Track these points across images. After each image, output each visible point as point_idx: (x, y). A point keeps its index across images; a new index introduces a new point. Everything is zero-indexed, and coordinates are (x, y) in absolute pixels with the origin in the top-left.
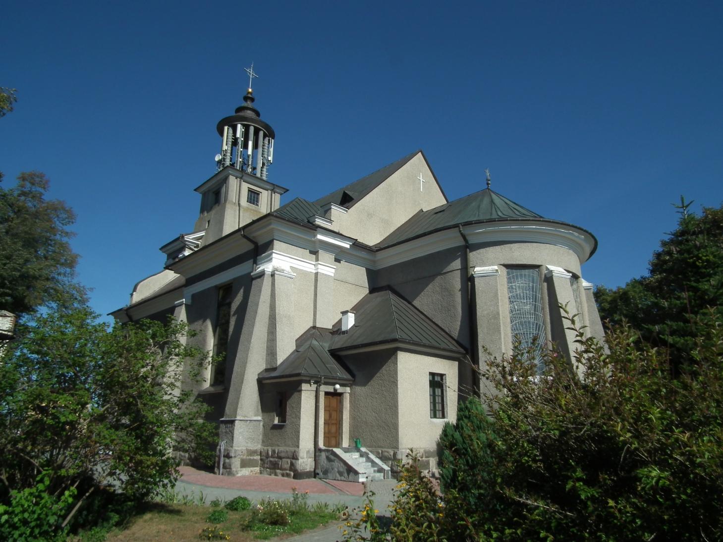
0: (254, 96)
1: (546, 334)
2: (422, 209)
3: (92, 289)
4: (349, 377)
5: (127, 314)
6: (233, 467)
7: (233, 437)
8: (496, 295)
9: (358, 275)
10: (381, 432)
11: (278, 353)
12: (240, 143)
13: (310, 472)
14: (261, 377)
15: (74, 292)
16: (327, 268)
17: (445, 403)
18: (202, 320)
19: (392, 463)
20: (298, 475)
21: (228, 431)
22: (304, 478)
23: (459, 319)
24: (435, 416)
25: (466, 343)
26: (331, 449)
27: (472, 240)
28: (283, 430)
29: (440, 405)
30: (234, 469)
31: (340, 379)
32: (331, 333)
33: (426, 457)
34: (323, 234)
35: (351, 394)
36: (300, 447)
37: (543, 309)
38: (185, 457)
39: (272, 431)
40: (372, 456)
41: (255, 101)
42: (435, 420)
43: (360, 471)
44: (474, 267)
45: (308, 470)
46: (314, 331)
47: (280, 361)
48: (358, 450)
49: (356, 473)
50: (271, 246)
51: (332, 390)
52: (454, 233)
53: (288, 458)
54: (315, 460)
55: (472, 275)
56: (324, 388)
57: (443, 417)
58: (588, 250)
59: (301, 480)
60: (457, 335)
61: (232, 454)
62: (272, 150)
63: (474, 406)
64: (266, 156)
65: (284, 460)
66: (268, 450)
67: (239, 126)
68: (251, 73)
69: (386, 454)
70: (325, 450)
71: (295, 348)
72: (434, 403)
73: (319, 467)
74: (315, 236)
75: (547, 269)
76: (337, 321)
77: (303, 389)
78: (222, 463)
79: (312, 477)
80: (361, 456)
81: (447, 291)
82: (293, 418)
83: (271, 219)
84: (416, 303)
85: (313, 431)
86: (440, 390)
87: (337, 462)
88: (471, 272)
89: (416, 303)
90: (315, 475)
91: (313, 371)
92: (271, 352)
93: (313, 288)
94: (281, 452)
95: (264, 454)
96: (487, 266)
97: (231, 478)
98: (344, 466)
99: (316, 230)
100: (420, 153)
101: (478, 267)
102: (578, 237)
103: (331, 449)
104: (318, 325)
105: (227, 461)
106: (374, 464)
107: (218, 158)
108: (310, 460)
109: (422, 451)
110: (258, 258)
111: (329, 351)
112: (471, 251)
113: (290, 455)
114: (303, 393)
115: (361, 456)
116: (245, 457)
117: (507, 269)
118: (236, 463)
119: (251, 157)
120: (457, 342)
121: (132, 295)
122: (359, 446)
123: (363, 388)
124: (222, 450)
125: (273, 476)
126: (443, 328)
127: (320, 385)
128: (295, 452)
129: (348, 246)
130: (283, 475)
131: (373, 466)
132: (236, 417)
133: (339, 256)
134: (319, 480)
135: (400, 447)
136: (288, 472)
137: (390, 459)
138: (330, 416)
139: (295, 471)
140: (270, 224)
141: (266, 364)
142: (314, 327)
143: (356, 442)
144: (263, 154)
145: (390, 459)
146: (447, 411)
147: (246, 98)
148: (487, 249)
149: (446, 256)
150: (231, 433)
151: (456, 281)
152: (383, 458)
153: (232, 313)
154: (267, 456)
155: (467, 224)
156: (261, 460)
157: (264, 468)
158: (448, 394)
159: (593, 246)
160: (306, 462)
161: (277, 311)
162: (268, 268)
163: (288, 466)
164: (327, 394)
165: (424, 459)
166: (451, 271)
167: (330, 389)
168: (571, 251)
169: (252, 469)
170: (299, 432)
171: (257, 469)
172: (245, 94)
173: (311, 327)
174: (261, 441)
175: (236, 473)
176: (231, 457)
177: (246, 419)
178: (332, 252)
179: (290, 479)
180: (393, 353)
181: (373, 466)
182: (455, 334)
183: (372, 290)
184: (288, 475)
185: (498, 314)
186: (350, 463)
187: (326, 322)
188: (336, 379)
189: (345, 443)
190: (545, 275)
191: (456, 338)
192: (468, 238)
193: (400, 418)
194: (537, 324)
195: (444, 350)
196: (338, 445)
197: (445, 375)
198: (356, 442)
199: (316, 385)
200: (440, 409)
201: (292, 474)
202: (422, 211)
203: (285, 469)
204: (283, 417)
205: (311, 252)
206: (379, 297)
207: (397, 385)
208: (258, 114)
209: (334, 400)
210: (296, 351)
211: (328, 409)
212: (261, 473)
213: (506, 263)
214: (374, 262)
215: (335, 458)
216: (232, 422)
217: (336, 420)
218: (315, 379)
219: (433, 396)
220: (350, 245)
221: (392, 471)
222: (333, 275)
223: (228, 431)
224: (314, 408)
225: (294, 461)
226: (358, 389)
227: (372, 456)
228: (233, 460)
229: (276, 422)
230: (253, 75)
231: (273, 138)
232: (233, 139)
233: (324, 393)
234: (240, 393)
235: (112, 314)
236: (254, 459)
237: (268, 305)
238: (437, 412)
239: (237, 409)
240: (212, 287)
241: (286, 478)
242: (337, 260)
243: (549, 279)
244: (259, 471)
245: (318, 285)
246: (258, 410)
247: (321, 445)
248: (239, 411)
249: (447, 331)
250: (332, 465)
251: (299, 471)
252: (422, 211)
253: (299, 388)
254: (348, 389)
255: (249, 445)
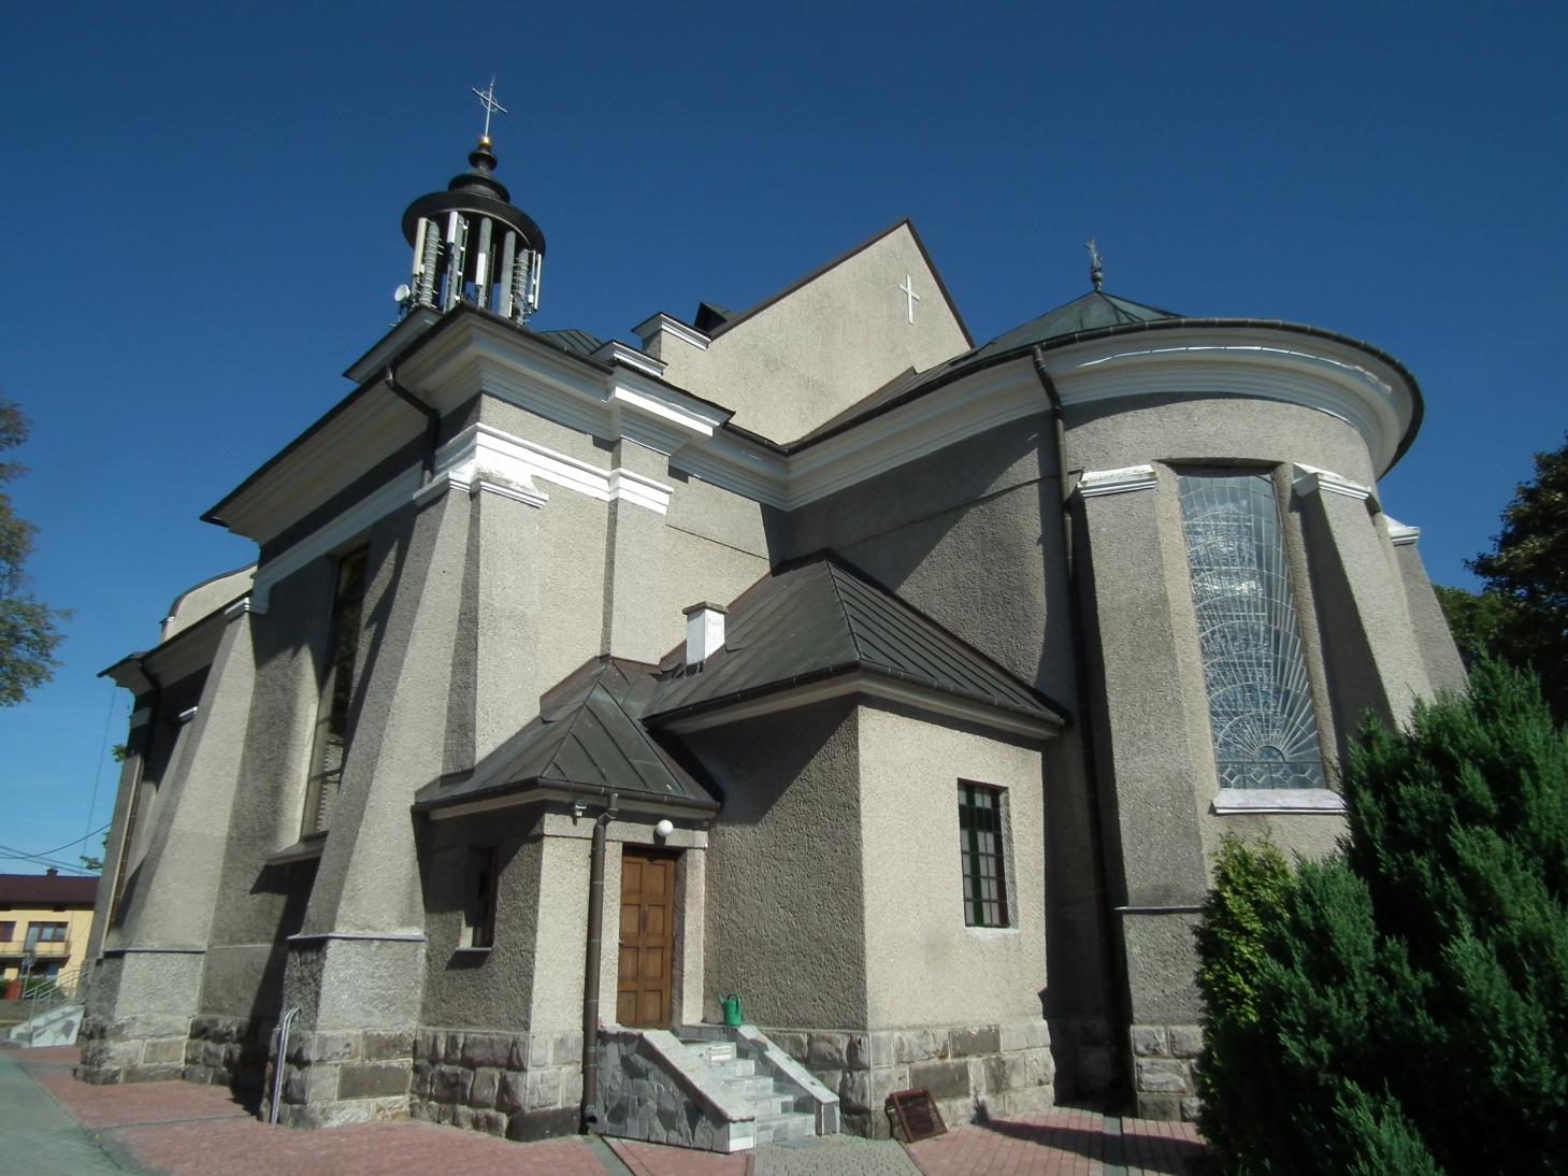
0: (495, 153)
1: (1306, 662)
2: (912, 369)
3: (67, 614)
4: (704, 797)
5: (144, 671)
6: (310, 1095)
7: (318, 994)
8: (1154, 544)
9: (739, 520)
10: (807, 981)
11: (479, 725)
12: (457, 257)
13: (566, 1112)
14: (423, 799)
15: (20, 620)
16: (645, 489)
17: (1007, 880)
18: (289, 652)
19: (844, 1080)
20: (523, 1127)
21: (306, 974)
22: (543, 1137)
23: (1040, 622)
24: (978, 920)
25: (1065, 695)
26: (636, 1031)
27: (1071, 395)
28: (482, 970)
29: (993, 884)
30: (314, 1105)
31: (672, 804)
32: (654, 675)
33: (958, 1055)
34: (632, 387)
35: (709, 852)
36: (535, 1025)
37: (1292, 589)
38: (217, 1056)
39: (452, 973)
40: (777, 1055)
41: (499, 165)
42: (978, 931)
43: (732, 1114)
44: (1081, 472)
45: (560, 1106)
46: (606, 668)
47: (483, 750)
48: (732, 1034)
49: (720, 1119)
50: (474, 414)
51: (649, 840)
52: (1019, 375)
53: (495, 1064)
54: (584, 1071)
55: (1077, 490)
56: (620, 832)
57: (1004, 922)
58: (1394, 436)
59: (531, 1145)
60: (1034, 673)
61: (312, 1054)
62: (536, 282)
63: (197, 1129)
64: (522, 293)
65: (480, 1070)
66: (435, 1038)
67: (454, 216)
68: (489, 100)
69: (824, 1047)
70: (617, 1037)
71: (537, 712)
72: (974, 878)
73: (599, 1094)
74: (608, 392)
75: (1299, 472)
76: (676, 645)
77: (547, 831)
78: (280, 1082)
79: (573, 1133)
80: (742, 1054)
81: (1004, 549)
82: (513, 928)
83: (470, 325)
84: (906, 590)
85: (582, 973)
86: (990, 837)
87: (658, 1079)
88: (1071, 484)
89: (906, 590)
90: (583, 1122)
91: (583, 775)
92: (461, 725)
93: (603, 544)
94: (475, 1043)
95: (424, 1050)
96: (1115, 465)
97: (304, 1137)
98: (677, 1092)
99: (611, 373)
100: (905, 225)
101: (1092, 470)
102: (1376, 387)
103: (636, 1031)
104: (616, 652)
105: (296, 1075)
106: (782, 1080)
107: (402, 293)
108: (566, 1069)
109: (942, 1034)
110: (438, 452)
111: (645, 721)
112: (1068, 427)
113: (501, 1053)
114: (549, 849)
115: (742, 1054)
116: (357, 1062)
117: (1179, 473)
118: (323, 1083)
119: (482, 292)
120: (1038, 695)
121: (164, 623)
122: (736, 1020)
123: (749, 829)
124: (285, 1038)
125: (446, 1128)
126: (991, 655)
127: (606, 822)
128: (514, 1044)
129: (709, 431)
130: (476, 1124)
131: (779, 1090)
132: (332, 929)
133: (685, 458)
134: (598, 1141)
135: (871, 1023)
136: (492, 1112)
137: (834, 1064)
138: (643, 922)
139: (513, 1109)
140: (468, 342)
141: (445, 762)
142: (605, 658)
143: (725, 1007)
144: (513, 287)
145: (834, 1064)
146: (1015, 905)
147: (475, 159)
148: (1119, 417)
149: (998, 446)
150: (314, 979)
151: (1027, 517)
152: (812, 1061)
153: (364, 622)
154: (434, 1060)
155: (1053, 344)
156: (416, 1069)
157: (422, 1096)
158: (1016, 852)
159: (1409, 416)
160: (551, 1079)
161: (482, 598)
162: (462, 474)
163: (490, 1093)
164: (630, 850)
165: (949, 1060)
166: (1011, 489)
167: (642, 834)
168: (1355, 432)
169: (380, 1100)
170: (530, 976)
171: (402, 1101)
172: (473, 148)
173: (596, 657)
174: (419, 1007)
175: (319, 1117)
176: (308, 1063)
177: (370, 934)
178: (659, 445)
179: (497, 1139)
180: (842, 712)
181: (779, 1090)
182: (1030, 671)
183: (779, 566)
184: (491, 1125)
185: (1164, 599)
186: (699, 1081)
187: (643, 644)
188: (659, 802)
189: (692, 1011)
190: (1294, 491)
191: (1032, 682)
192: (1060, 388)
193: (869, 924)
194: (1277, 633)
195: (1003, 710)
196: (666, 1019)
197: (1006, 788)
198: (725, 1007)
199: (592, 822)
200: (994, 896)
201: (504, 1120)
202: (912, 369)
203: (484, 1105)
204: (483, 921)
205: (599, 443)
206: (798, 578)
207: (857, 816)
208: (503, 194)
209: (655, 873)
210: (543, 720)
211: (634, 899)
212: (412, 1114)
213: (1175, 456)
214: (785, 487)
215: (650, 1065)
216: (319, 945)
217: (663, 934)
218: (592, 801)
219: (972, 854)
220: (715, 429)
221: (846, 1106)
222: (663, 510)
223: (306, 974)
224: (585, 896)
225: (510, 1075)
226: (736, 835)
227: (777, 1055)
228: (313, 1073)
229: (466, 942)
230: (493, 106)
231: (542, 251)
232: (439, 249)
233: (620, 847)
234: (351, 853)
235: (109, 672)
236: (390, 1069)
237: (458, 582)
238: (985, 907)
239: (337, 903)
240: (320, 557)
241: (483, 1135)
242: (677, 473)
243: (1308, 503)
244: (406, 1108)
245: (619, 534)
246: (412, 908)
247: (608, 1018)
248: (344, 909)
249: (1003, 663)
250: (640, 1089)
251: (528, 1111)
252: (912, 369)
253: (536, 831)
254: (701, 838)
255: (376, 1020)
